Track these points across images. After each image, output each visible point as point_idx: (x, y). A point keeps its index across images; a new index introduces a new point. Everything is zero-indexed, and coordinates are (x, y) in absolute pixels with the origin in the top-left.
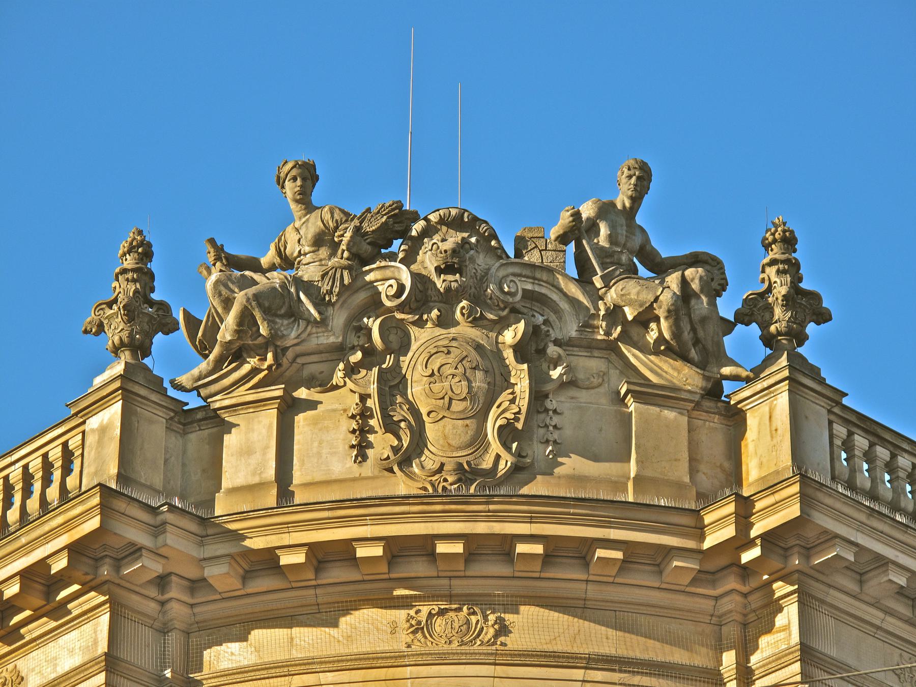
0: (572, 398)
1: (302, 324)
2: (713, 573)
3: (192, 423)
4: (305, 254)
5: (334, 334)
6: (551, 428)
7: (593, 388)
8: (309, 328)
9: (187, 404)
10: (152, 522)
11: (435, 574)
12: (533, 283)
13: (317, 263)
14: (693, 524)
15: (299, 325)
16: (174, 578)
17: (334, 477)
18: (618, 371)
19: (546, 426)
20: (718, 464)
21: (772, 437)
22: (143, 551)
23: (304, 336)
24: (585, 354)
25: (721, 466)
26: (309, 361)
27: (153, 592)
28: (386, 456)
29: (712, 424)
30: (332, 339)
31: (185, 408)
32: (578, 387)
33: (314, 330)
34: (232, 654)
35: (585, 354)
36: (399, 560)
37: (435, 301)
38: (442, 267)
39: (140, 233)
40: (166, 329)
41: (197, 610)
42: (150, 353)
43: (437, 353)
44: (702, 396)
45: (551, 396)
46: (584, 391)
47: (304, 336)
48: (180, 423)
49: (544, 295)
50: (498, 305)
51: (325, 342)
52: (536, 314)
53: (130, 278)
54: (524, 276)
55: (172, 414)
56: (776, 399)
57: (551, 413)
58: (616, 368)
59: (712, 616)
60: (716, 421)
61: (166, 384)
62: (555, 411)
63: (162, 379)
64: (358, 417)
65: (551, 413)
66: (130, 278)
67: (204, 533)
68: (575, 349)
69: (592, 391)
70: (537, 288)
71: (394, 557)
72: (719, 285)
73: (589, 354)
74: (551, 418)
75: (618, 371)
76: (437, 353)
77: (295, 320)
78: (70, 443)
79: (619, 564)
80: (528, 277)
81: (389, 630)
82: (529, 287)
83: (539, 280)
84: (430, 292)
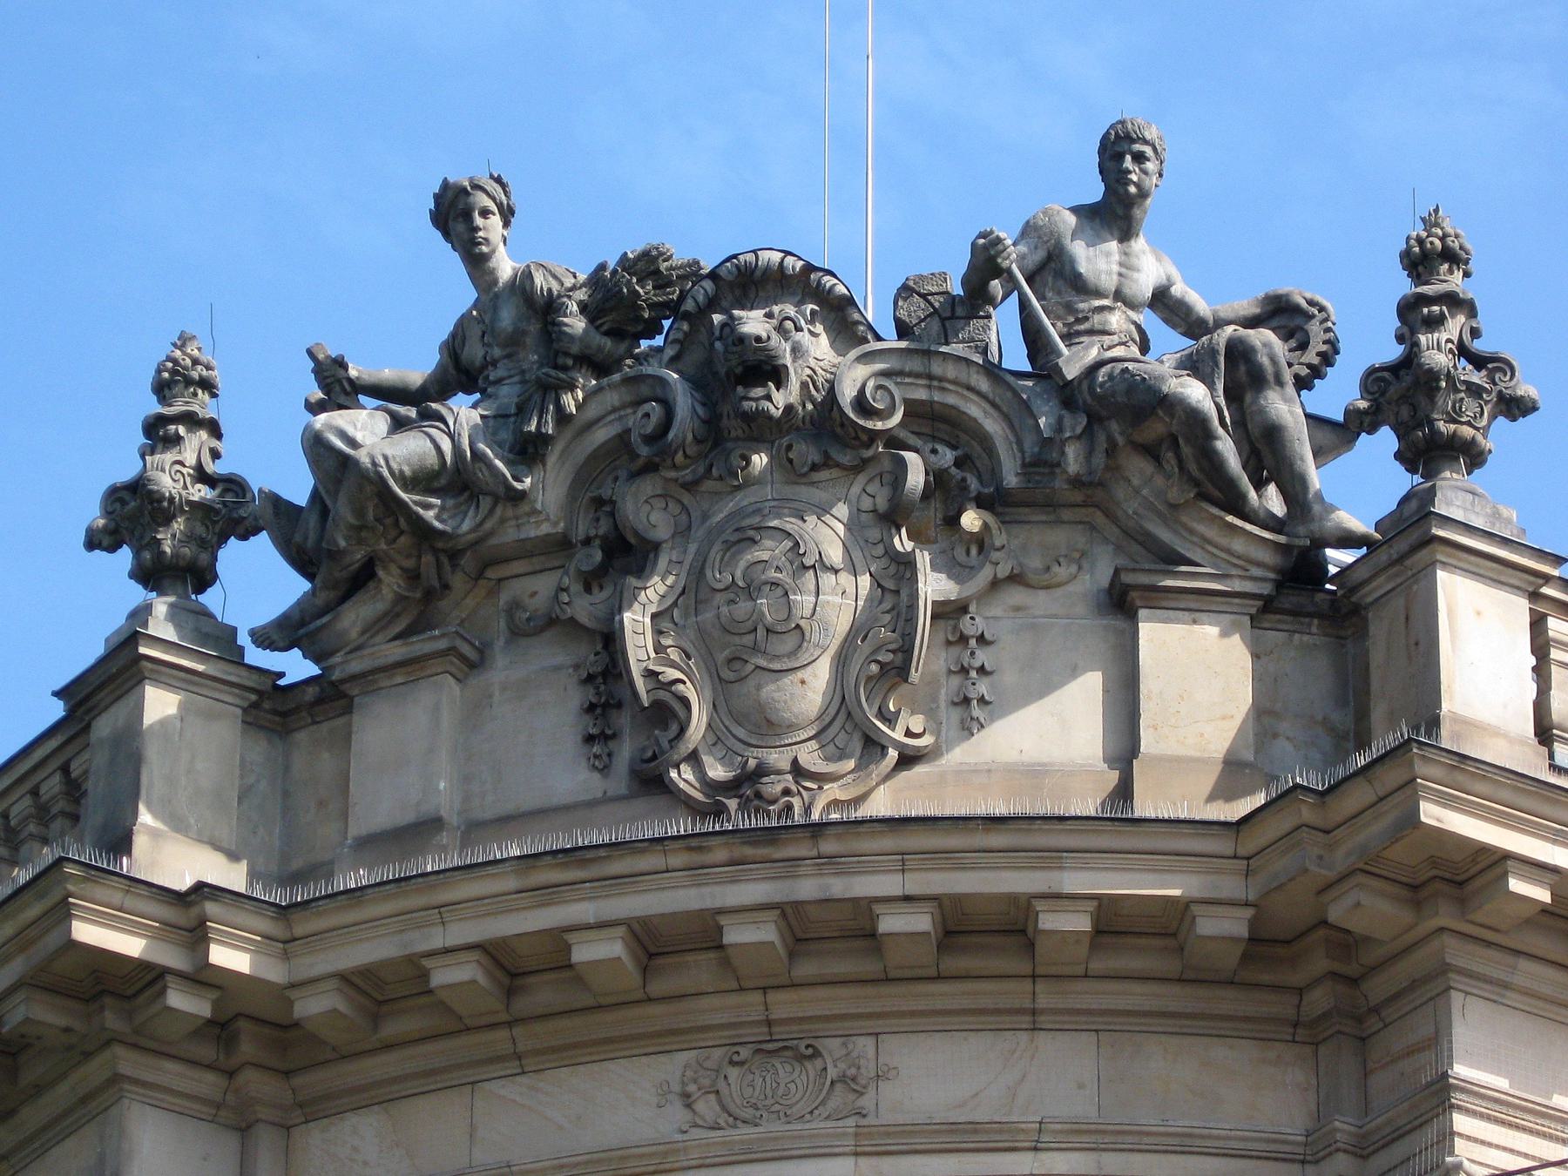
0: (1017, 609)
1: (486, 503)
2: (1288, 942)
3: (297, 709)
4: (494, 363)
5: (548, 519)
6: (973, 674)
7: (1059, 585)
8: (499, 511)
9: (281, 675)
10: (183, 922)
11: (735, 985)
12: (929, 387)
13: (516, 379)
14: (1230, 852)
15: (478, 506)
16: (242, 1024)
17: (555, 801)
18: (1110, 548)
19: (964, 671)
20: (1320, 718)
21: (1410, 658)
22: (169, 978)
23: (488, 525)
24: (1044, 518)
25: (1325, 721)
26: (508, 574)
27: (207, 1052)
28: (649, 754)
29: (1306, 638)
30: (545, 529)
31: (282, 682)
32: (1028, 585)
33: (510, 512)
34: (365, 1163)
35: (1044, 518)
36: (660, 961)
37: (737, 439)
38: (739, 370)
39: (1436, 211)
40: (241, 529)
41: (298, 1081)
42: (215, 577)
43: (739, 541)
44: (1279, 585)
45: (972, 608)
46: (1042, 593)
47: (488, 525)
48: (275, 712)
49: (953, 407)
50: (857, 438)
51: (532, 534)
52: (939, 447)
53: (1458, 275)
54: (910, 375)
55: (253, 697)
56: (1416, 582)
57: (973, 642)
58: (1106, 541)
59: (1295, 1025)
60: (1314, 630)
61: (244, 639)
62: (981, 639)
63: (235, 630)
64: (600, 680)
65: (973, 642)
66: (1458, 275)
67: (288, 936)
68: (1021, 510)
69: (1059, 592)
70: (937, 397)
71: (651, 956)
72: (1318, 354)
73: (1052, 517)
74: (973, 654)
75: (1110, 548)
76: (739, 541)
77: (471, 498)
78: (73, 766)
79: (1086, 941)
80: (918, 376)
81: (654, 1100)
82: (921, 394)
83: (941, 380)
84: (725, 421)
